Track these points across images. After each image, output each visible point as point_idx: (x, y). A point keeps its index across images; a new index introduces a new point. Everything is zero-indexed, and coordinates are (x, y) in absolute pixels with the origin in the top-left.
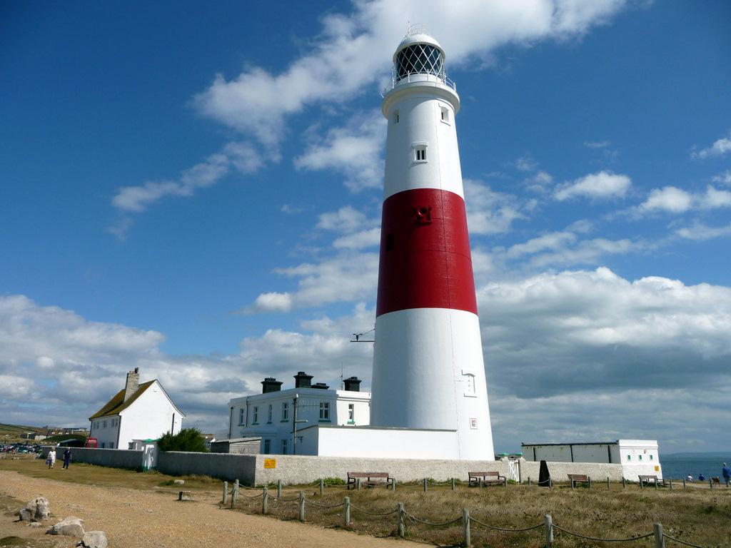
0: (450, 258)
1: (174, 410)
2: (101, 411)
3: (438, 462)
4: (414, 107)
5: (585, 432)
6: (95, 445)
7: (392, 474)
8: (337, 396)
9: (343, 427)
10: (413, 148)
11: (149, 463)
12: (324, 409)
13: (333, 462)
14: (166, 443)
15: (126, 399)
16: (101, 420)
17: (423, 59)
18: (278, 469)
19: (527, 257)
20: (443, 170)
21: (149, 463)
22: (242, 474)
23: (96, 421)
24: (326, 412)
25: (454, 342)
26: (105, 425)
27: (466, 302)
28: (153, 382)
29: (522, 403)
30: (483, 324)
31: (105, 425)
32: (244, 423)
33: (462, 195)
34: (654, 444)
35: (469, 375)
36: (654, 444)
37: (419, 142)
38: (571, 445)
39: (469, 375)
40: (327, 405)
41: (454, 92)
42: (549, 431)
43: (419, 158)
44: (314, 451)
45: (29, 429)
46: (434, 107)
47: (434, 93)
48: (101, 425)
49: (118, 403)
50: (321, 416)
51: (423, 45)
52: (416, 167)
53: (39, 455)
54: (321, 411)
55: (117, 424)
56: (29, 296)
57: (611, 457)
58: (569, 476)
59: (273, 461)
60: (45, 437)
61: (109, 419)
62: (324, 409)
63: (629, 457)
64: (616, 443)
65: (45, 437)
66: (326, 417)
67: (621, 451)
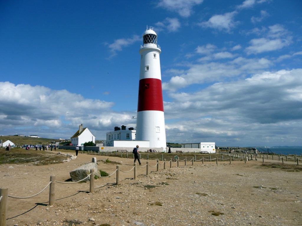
0: (155, 97)
1: (92, 135)
2: (73, 136)
3: (143, 148)
4: (148, 53)
5: (283, 137)
6: (73, 145)
7: (127, 150)
8: (132, 132)
9: (134, 140)
10: (145, 67)
11: (83, 149)
12: (128, 135)
13: (117, 148)
14: (86, 145)
15: (79, 133)
16: (73, 138)
17: (149, 39)
18: (107, 149)
19: (30, 160)
20: (155, 72)
21: (83, 149)
22: (97, 150)
23: (72, 138)
24: (129, 136)
25: (156, 119)
26: (75, 140)
27: (160, 108)
28: (86, 128)
29: (256, 125)
30: (165, 114)
31: (75, 140)
32: (119, 138)
33: (161, 80)
34: (214, 143)
35: (158, 127)
36: (214, 143)
37: (147, 65)
38: (191, 144)
39: (158, 127)
40: (129, 134)
41: (160, 50)
42: (267, 137)
43: (147, 70)
44: (113, 146)
45: (53, 140)
46: (152, 54)
47: (152, 50)
48: (74, 140)
49: (78, 134)
50: (127, 137)
51: (149, 34)
52: (146, 72)
53: (58, 148)
54: (127, 136)
55: (77, 139)
56: (46, 86)
57: (199, 147)
58: (176, 151)
59: (103, 148)
60: (59, 143)
61: (75, 138)
62: (128, 135)
63: (204, 147)
64: (200, 143)
65: (59, 143)
66: (129, 137)
67: (201, 145)
